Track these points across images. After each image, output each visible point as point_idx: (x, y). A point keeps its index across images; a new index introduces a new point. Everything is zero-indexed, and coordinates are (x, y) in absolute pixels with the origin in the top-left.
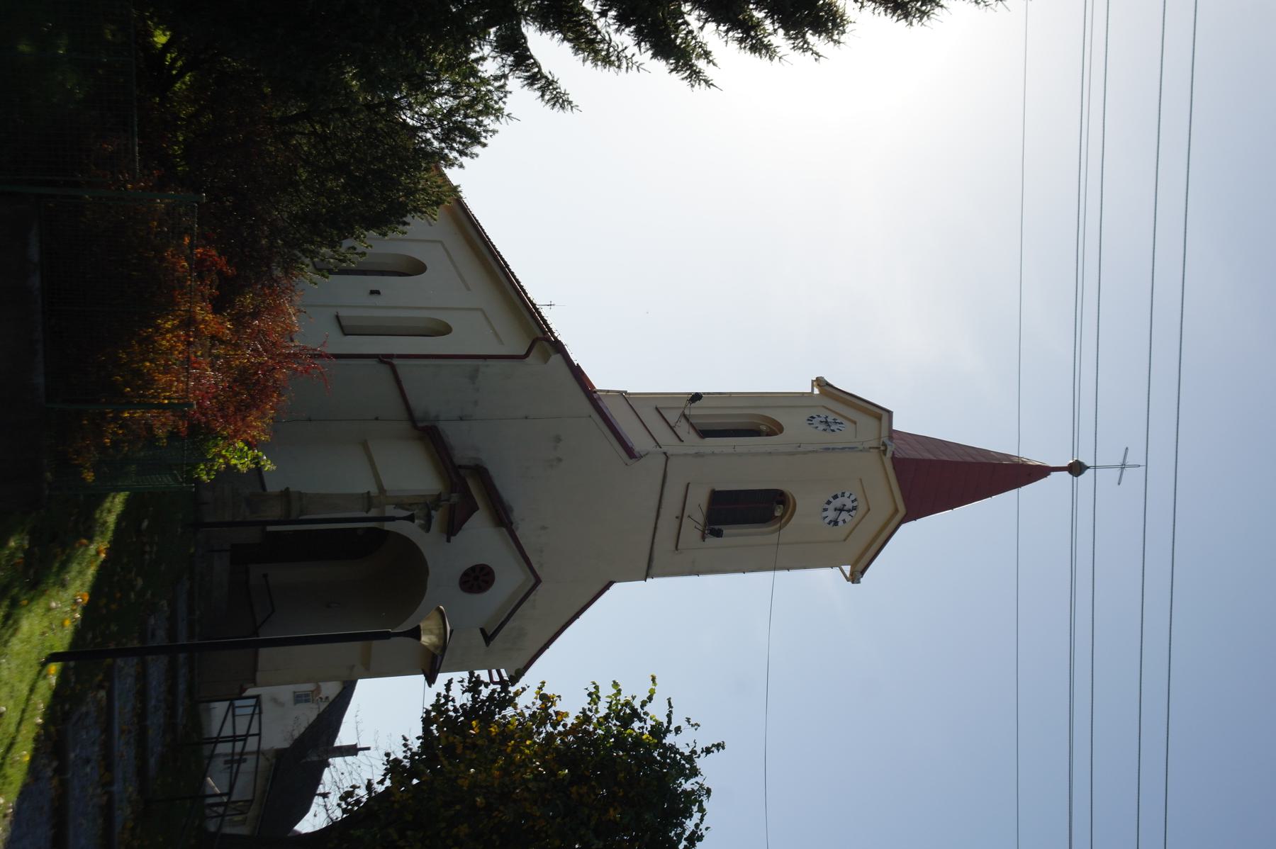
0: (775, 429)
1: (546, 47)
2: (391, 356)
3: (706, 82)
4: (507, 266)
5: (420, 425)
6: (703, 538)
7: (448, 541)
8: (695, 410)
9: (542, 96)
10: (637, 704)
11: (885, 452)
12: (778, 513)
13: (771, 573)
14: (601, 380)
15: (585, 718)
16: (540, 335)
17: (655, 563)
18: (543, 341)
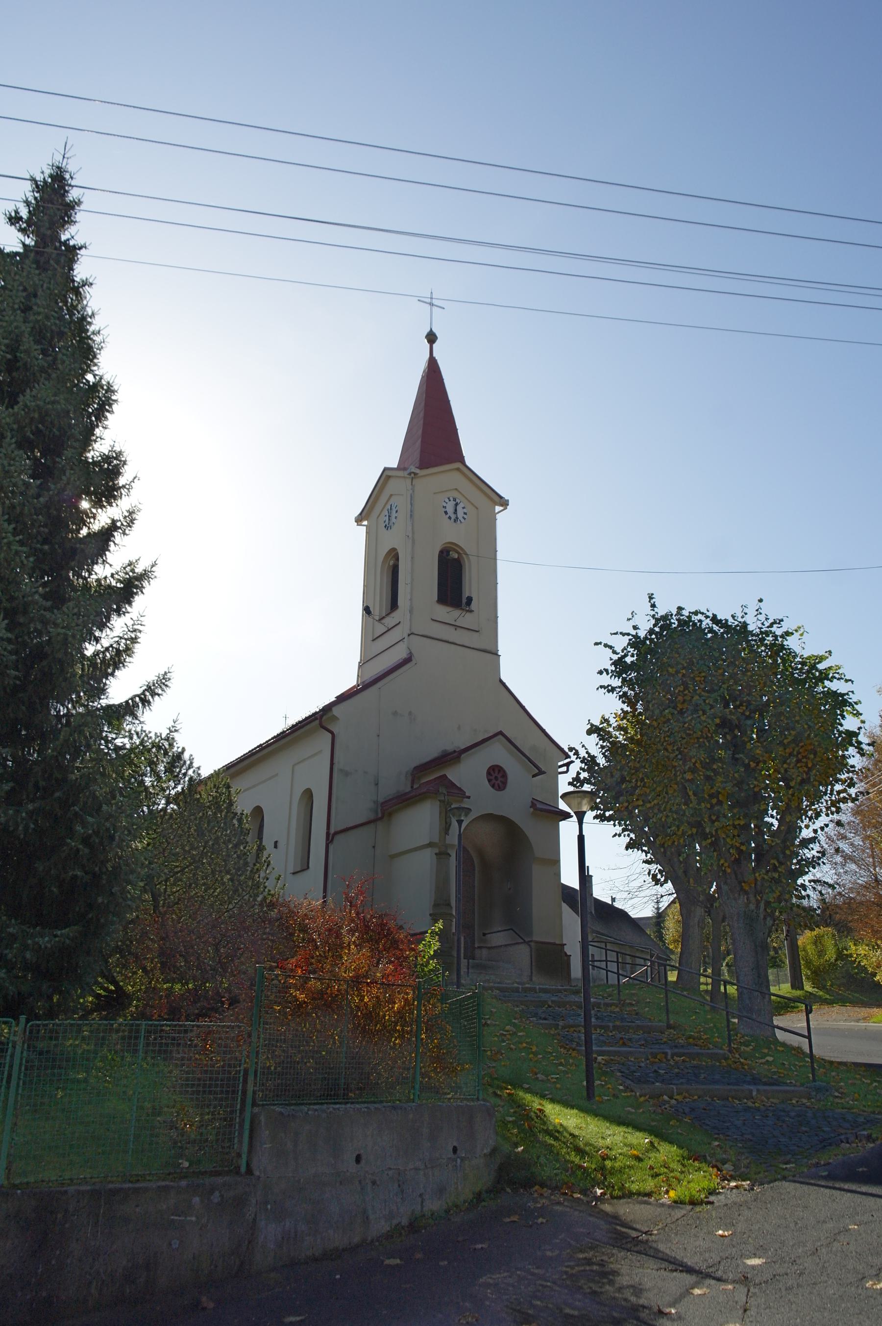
0: (394, 554)
1: (119, 689)
2: (328, 834)
3: (153, 566)
4: (261, 745)
5: (380, 815)
6: (471, 611)
7: (469, 797)
8: (376, 611)
9: (159, 695)
10: (615, 657)
11: (415, 474)
12: (456, 556)
13: (499, 562)
14: (349, 680)
15: (624, 697)
16: (317, 722)
17: (488, 648)
18: (321, 720)
